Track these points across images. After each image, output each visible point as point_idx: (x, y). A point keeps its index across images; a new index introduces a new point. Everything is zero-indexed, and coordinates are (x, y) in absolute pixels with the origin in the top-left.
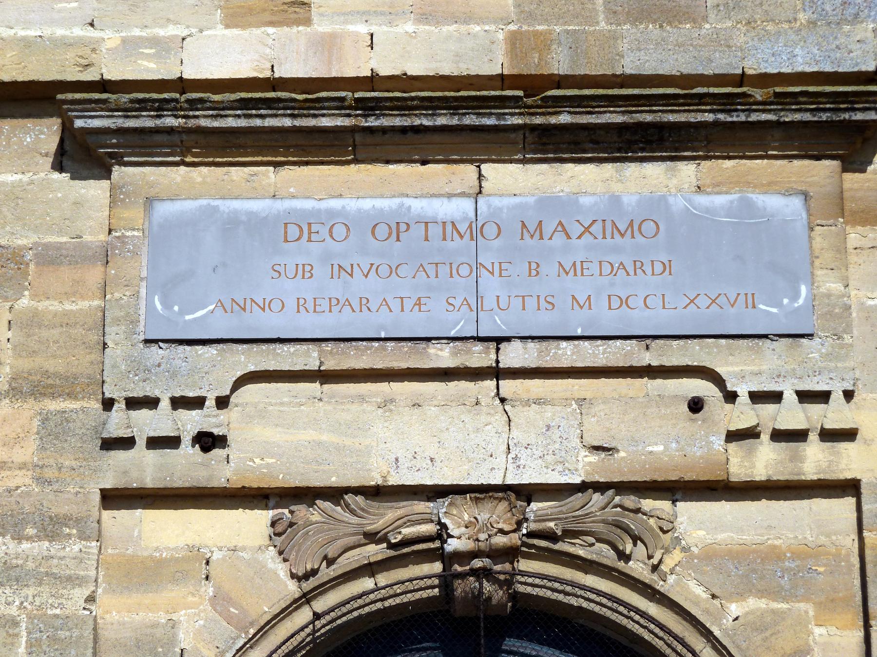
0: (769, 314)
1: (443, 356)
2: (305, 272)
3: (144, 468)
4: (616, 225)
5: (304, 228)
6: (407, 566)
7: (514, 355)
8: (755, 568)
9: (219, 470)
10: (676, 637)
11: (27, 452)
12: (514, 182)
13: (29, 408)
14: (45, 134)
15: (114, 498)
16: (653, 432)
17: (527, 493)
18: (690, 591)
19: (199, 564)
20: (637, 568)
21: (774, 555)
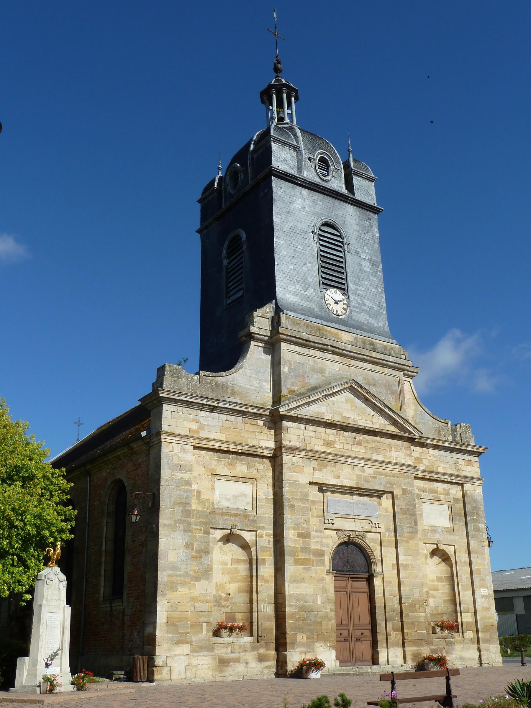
0: (375, 515)
1: (351, 517)
2: (340, 506)
3: (327, 526)
4: (364, 504)
5: (339, 501)
6: (69, 602)
7: (356, 517)
8: (373, 540)
9: (334, 527)
10: (434, 480)
11: (318, 524)
12: (356, 498)
13: (318, 518)
14: (316, 487)
15: (325, 529)
16: (367, 527)
17: (356, 531)
18: (368, 542)
19: (330, 537)
20: (364, 539)
21: (374, 539)
